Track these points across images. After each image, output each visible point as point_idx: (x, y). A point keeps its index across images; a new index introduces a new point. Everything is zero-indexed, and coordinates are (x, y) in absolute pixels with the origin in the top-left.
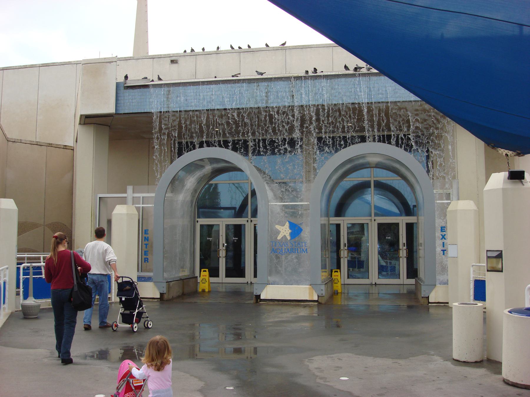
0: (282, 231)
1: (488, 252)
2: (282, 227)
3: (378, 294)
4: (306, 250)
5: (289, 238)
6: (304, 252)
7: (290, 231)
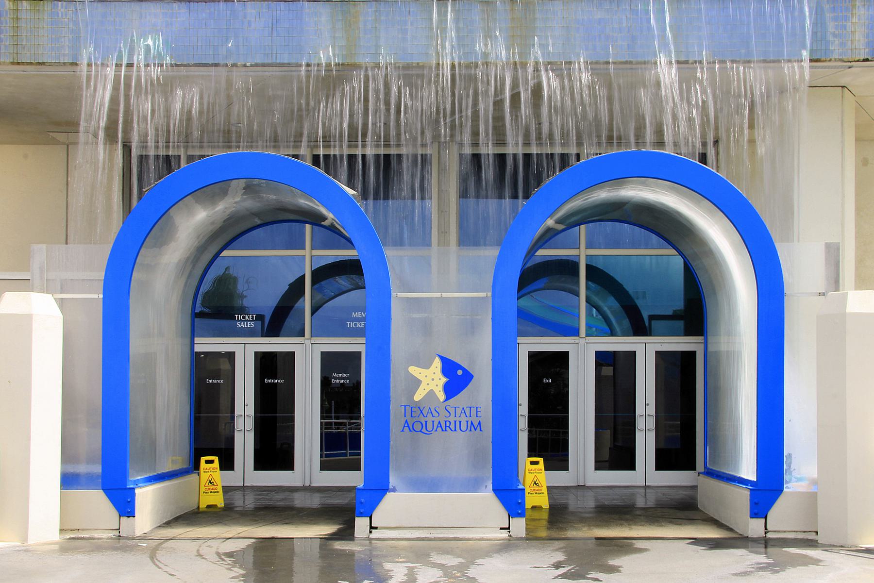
0: (425, 381)
1: (508, 527)
2: (424, 371)
3: (376, 528)
4: (480, 423)
5: (442, 396)
6: (475, 429)
7: (444, 380)
